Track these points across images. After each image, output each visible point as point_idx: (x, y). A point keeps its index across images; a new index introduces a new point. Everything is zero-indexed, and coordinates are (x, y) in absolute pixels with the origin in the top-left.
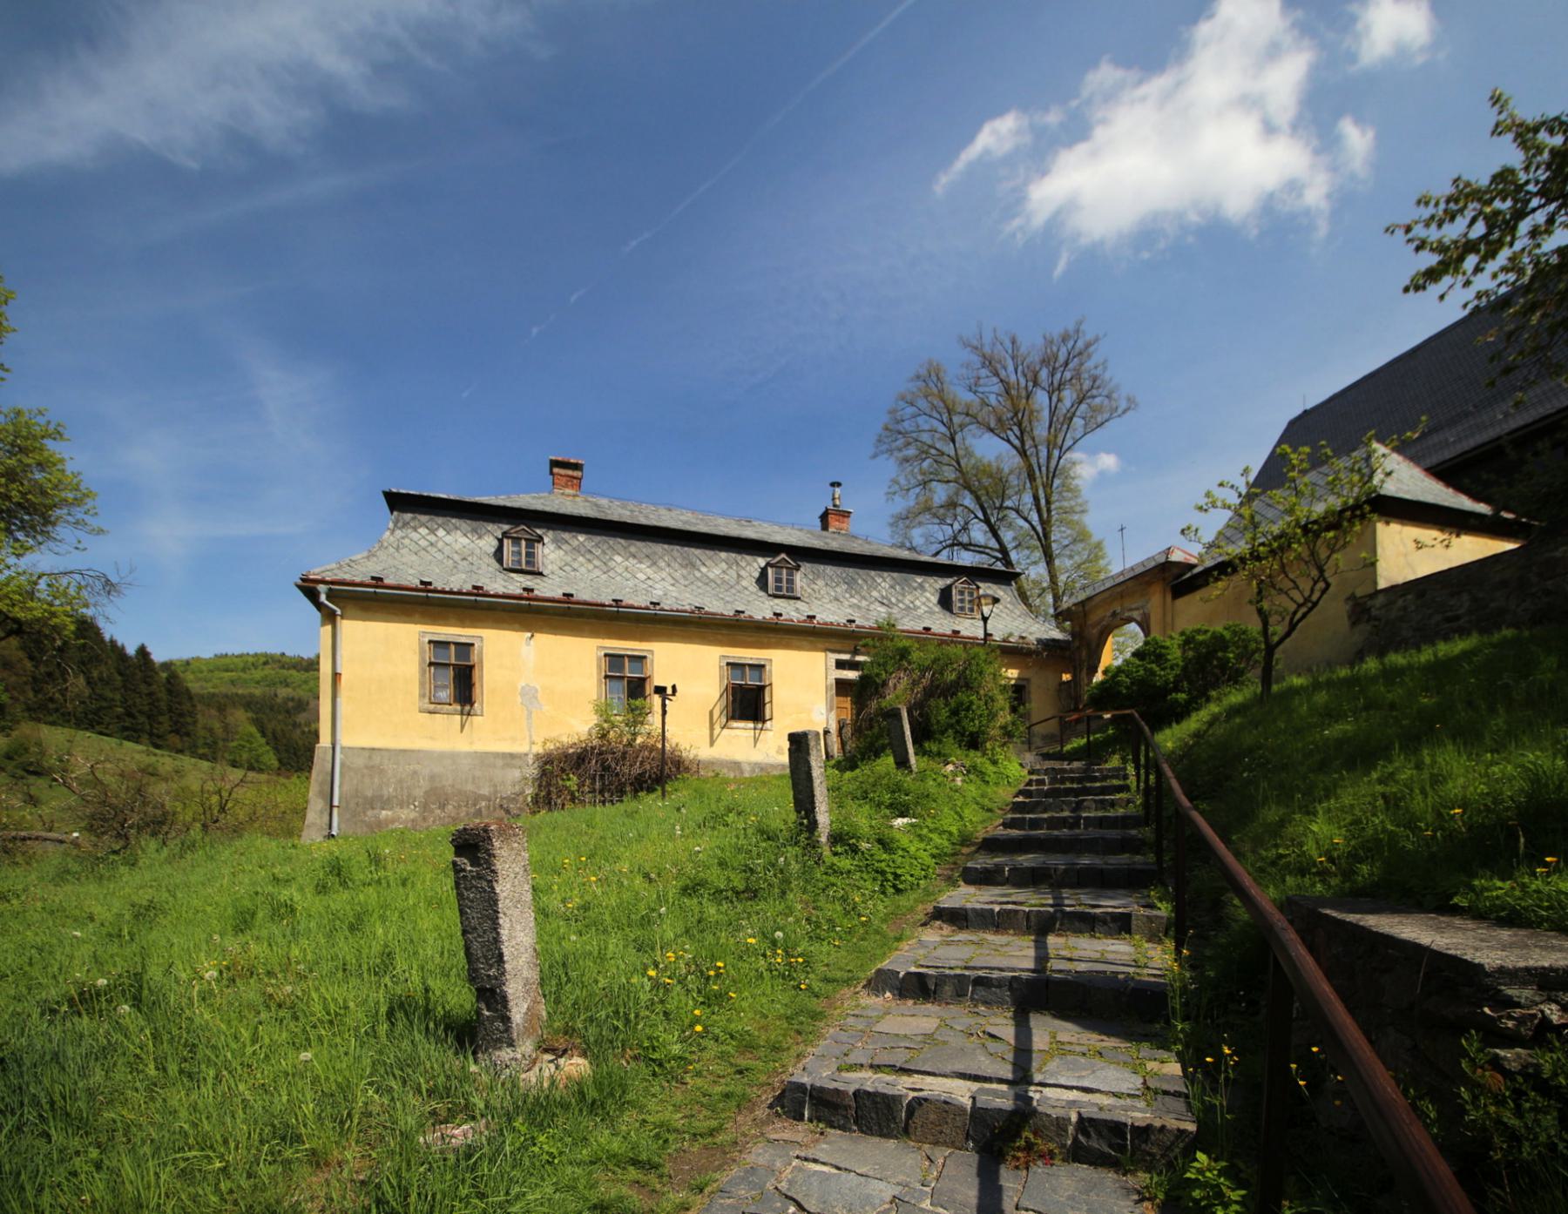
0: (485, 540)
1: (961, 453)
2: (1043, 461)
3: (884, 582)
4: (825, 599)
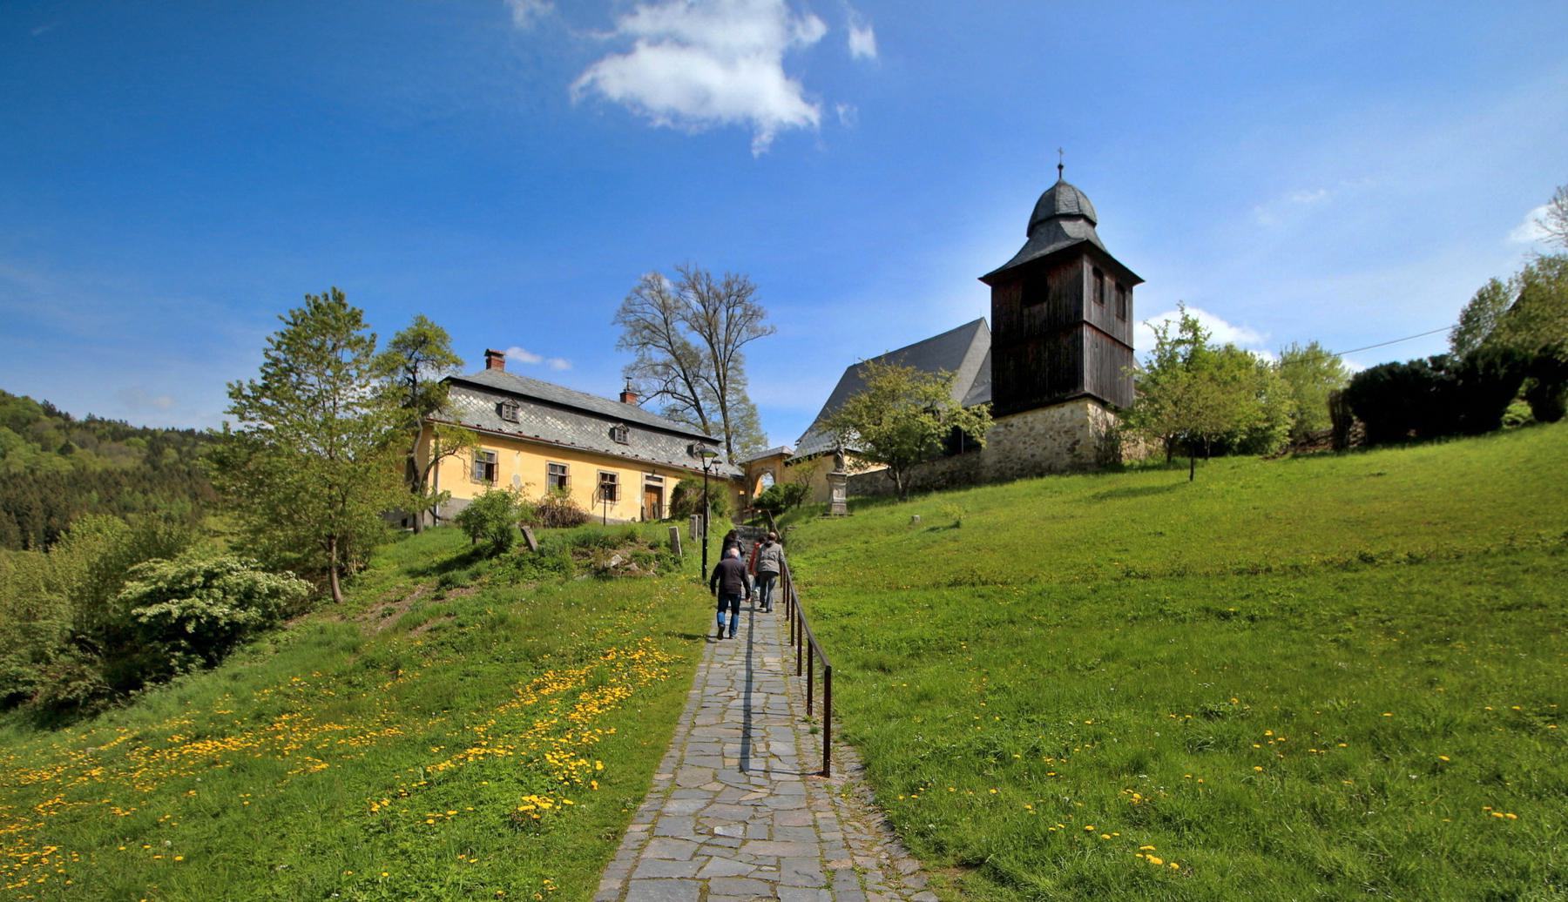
3: (664, 439)
4: (640, 446)
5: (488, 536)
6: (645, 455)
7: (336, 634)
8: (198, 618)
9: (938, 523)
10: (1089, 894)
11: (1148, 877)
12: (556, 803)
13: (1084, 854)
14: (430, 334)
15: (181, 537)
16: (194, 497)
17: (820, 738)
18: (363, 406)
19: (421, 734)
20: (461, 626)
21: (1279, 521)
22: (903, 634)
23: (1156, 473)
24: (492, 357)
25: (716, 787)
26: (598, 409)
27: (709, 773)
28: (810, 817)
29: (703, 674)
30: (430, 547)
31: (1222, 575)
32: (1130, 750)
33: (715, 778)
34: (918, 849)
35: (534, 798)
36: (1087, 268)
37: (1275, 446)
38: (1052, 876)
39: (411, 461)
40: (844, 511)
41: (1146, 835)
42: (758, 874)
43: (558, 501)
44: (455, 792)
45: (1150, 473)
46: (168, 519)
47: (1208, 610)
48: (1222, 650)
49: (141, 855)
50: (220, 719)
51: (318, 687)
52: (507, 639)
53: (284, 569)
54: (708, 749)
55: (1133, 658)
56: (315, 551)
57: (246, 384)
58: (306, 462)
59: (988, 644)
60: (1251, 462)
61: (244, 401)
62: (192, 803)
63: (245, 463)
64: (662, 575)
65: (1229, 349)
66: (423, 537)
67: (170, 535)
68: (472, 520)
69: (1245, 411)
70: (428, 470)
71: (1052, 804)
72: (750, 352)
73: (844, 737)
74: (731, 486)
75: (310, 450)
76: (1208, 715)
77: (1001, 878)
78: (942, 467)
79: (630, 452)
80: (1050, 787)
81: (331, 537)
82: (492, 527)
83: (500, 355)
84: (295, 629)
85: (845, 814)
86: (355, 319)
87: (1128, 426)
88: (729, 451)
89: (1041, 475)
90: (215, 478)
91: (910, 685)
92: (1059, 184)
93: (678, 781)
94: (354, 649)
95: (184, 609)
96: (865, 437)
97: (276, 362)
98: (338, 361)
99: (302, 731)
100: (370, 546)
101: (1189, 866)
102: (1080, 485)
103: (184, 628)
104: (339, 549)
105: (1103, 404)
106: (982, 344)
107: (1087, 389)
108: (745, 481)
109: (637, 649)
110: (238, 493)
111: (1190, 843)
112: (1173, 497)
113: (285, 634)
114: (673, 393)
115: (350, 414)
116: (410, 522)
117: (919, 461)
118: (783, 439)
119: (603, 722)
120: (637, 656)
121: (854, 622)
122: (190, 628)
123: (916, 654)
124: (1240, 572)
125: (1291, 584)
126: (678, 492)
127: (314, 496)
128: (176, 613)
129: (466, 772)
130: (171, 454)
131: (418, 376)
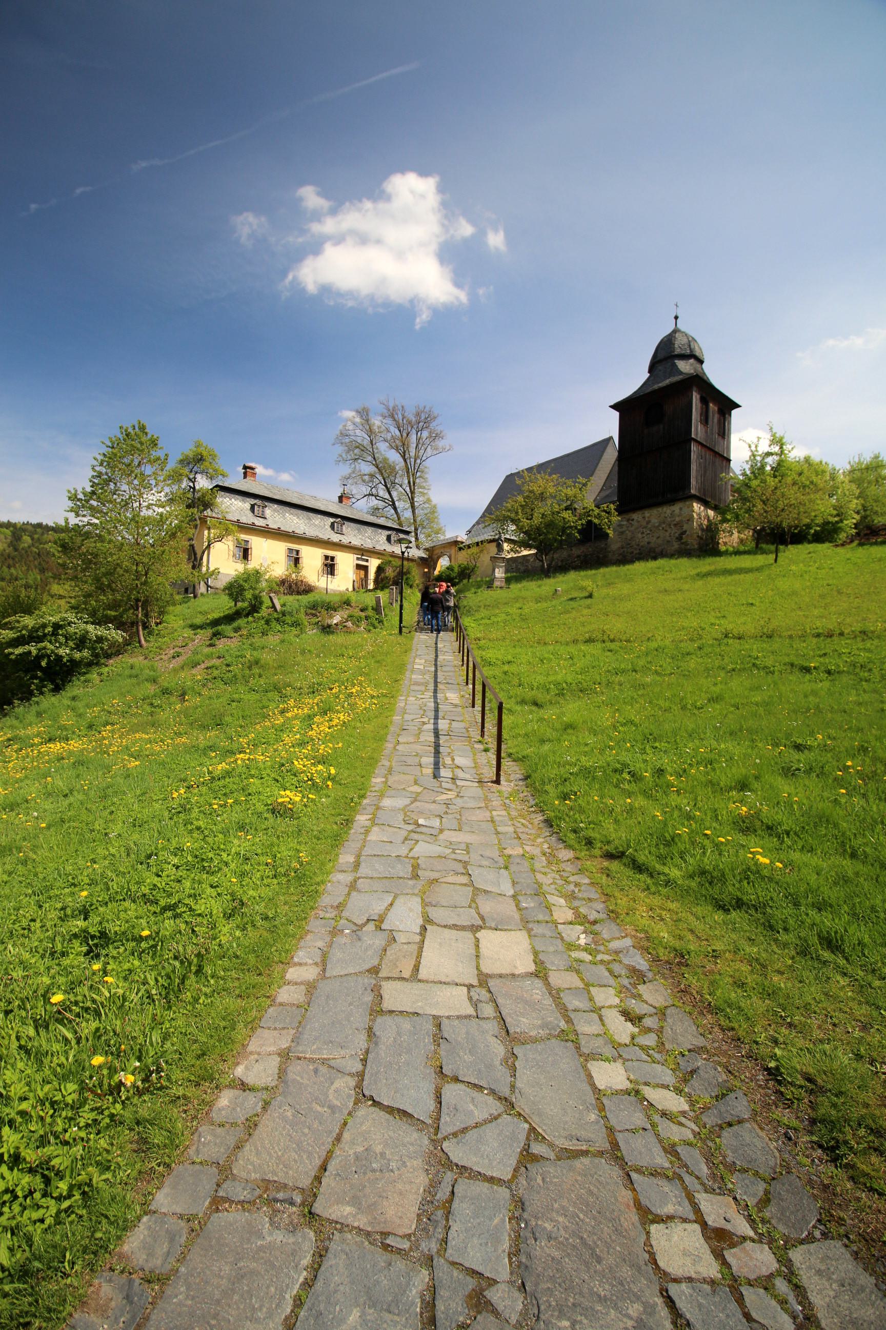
0: (246, 504)
1: (376, 451)
2: (413, 463)
4: (352, 535)
5: (246, 602)
6: (356, 542)
7: (141, 670)
8: (49, 656)
9: (575, 594)
10: (710, 883)
11: (758, 872)
12: (303, 797)
13: (704, 853)
14: (205, 454)
15: (35, 600)
16: (42, 571)
17: (493, 757)
18: (159, 506)
19: (202, 743)
20: (228, 665)
21: (848, 595)
22: (551, 678)
23: (746, 556)
24: (248, 471)
25: (418, 789)
26: (322, 508)
27: (411, 778)
28: (488, 814)
29: (402, 705)
30: (205, 608)
31: (803, 637)
32: (738, 772)
33: (416, 783)
34: (572, 842)
35: (288, 792)
36: (696, 397)
37: (843, 536)
38: (680, 869)
39: (192, 546)
40: (503, 584)
41: (752, 839)
42: (453, 856)
43: (294, 576)
44: (231, 786)
45: (742, 557)
46: (27, 586)
47: (792, 665)
48: (806, 696)
49: (17, 822)
50: (64, 728)
51: (130, 707)
52: (260, 676)
53: (106, 623)
54: (410, 761)
55: (733, 702)
56: (125, 611)
57: (80, 490)
58: (120, 548)
59: (617, 687)
60: (824, 548)
61: (79, 503)
62: (49, 786)
63: (79, 548)
64: (369, 631)
65: (807, 460)
66: (200, 600)
67: (29, 597)
68: (235, 589)
69: (822, 508)
70: (203, 553)
71: (676, 814)
72: (433, 465)
73: (510, 755)
74: (418, 565)
75: (123, 538)
76: (798, 747)
77: (639, 868)
78: (576, 551)
79: (345, 540)
80: (674, 799)
81: (137, 600)
82: (248, 595)
83: (253, 469)
84: (114, 665)
85: (514, 813)
86: (154, 443)
87: (724, 520)
88: (417, 539)
89: (655, 558)
90: (59, 557)
91: (558, 717)
92: (676, 331)
93: (389, 783)
94: (154, 681)
95: (39, 650)
96: (520, 529)
97: (100, 475)
98: (142, 474)
99: (120, 737)
100: (163, 607)
101: (789, 864)
102: (686, 566)
103: (40, 663)
104: (143, 609)
105: (706, 504)
106: (611, 455)
107: (693, 491)
108: (429, 562)
109: (353, 685)
110: (75, 568)
111: (789, 847)
112: (762, 576)
113: (107, 669)
114: (376, 496)
115: (150, 512)
116: (190, 590)
117: (560, 547)
118: (456, 530)
119: (332, 738)
120: (354, 690)
121: (513, 668)
122: (44, 664)
123: (561, 694)
124: (818, 635)
125: (860, 645)
126: (380, 569)
127: (127, 571)
128: (34, 652)
129: (238, 771)
130: (27, 539)
131: (196, 484)
